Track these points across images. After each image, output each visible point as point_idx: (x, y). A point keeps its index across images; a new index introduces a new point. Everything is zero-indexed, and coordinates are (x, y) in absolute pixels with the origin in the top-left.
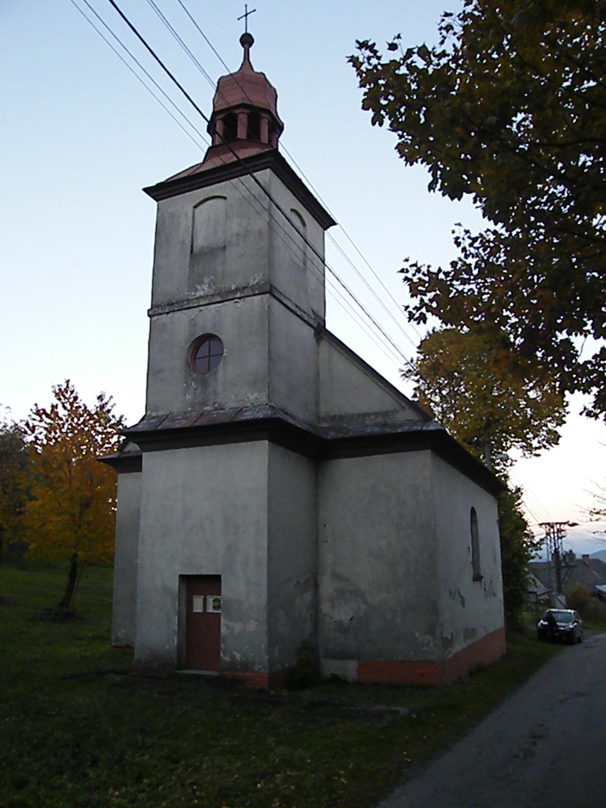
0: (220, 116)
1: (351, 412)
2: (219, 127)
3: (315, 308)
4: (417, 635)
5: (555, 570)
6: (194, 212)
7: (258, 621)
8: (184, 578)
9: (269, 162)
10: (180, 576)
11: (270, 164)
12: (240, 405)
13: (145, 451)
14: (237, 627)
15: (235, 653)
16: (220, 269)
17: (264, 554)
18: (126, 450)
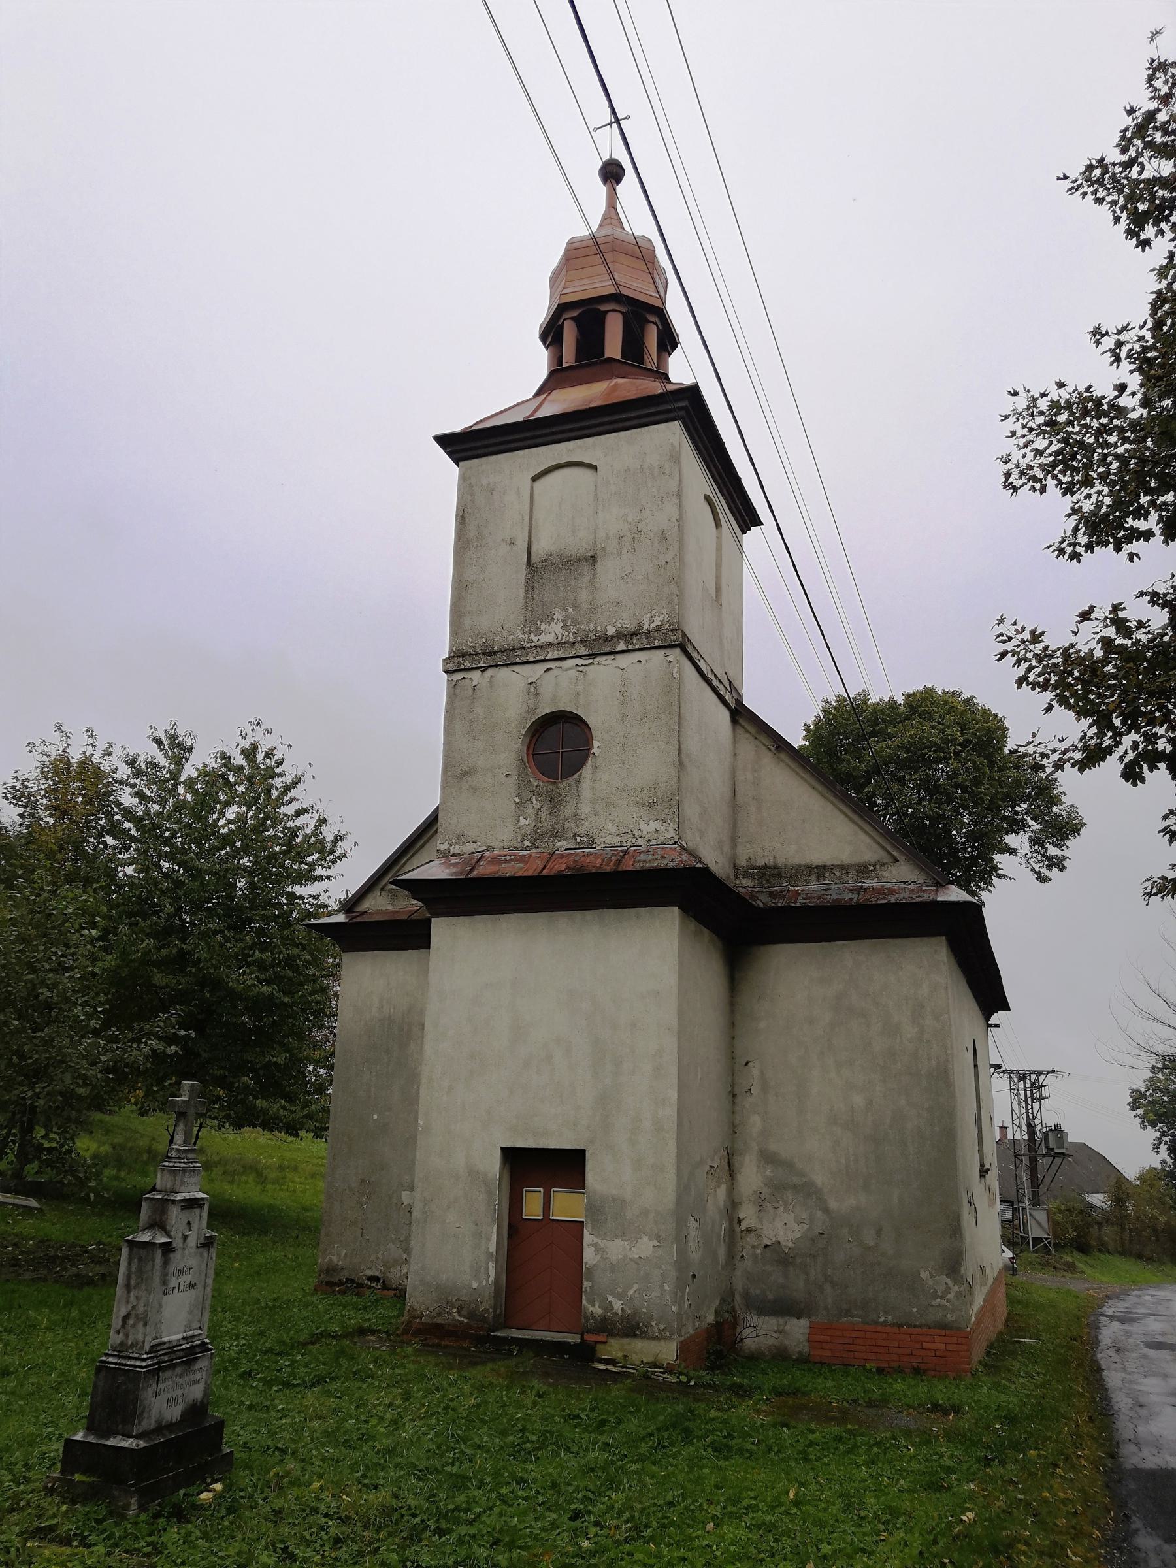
0: (575, 313)
1: (797, 861)
2: (570, 333)
3: (731, 675)
4: (924, 1275)
5: (1026, 1160)
6: (532, 488)
7: (658, 1238)
8: (511, 1156)
9: (681, 409)
10: (502, 1148)
11: (682, 413)
12: (627, 841)
13: (438, 915)
14: (616, 1249)
15: (610, 1298)
16: (584, 596)
17: (669, 1113)
18: (357, 910)
